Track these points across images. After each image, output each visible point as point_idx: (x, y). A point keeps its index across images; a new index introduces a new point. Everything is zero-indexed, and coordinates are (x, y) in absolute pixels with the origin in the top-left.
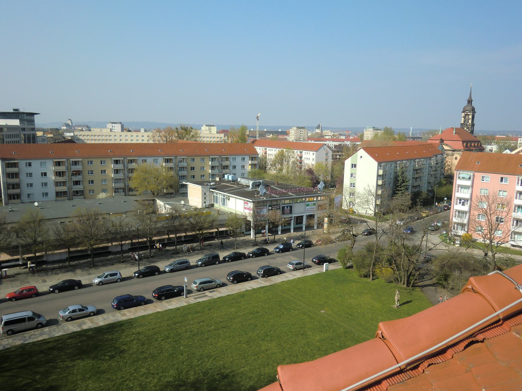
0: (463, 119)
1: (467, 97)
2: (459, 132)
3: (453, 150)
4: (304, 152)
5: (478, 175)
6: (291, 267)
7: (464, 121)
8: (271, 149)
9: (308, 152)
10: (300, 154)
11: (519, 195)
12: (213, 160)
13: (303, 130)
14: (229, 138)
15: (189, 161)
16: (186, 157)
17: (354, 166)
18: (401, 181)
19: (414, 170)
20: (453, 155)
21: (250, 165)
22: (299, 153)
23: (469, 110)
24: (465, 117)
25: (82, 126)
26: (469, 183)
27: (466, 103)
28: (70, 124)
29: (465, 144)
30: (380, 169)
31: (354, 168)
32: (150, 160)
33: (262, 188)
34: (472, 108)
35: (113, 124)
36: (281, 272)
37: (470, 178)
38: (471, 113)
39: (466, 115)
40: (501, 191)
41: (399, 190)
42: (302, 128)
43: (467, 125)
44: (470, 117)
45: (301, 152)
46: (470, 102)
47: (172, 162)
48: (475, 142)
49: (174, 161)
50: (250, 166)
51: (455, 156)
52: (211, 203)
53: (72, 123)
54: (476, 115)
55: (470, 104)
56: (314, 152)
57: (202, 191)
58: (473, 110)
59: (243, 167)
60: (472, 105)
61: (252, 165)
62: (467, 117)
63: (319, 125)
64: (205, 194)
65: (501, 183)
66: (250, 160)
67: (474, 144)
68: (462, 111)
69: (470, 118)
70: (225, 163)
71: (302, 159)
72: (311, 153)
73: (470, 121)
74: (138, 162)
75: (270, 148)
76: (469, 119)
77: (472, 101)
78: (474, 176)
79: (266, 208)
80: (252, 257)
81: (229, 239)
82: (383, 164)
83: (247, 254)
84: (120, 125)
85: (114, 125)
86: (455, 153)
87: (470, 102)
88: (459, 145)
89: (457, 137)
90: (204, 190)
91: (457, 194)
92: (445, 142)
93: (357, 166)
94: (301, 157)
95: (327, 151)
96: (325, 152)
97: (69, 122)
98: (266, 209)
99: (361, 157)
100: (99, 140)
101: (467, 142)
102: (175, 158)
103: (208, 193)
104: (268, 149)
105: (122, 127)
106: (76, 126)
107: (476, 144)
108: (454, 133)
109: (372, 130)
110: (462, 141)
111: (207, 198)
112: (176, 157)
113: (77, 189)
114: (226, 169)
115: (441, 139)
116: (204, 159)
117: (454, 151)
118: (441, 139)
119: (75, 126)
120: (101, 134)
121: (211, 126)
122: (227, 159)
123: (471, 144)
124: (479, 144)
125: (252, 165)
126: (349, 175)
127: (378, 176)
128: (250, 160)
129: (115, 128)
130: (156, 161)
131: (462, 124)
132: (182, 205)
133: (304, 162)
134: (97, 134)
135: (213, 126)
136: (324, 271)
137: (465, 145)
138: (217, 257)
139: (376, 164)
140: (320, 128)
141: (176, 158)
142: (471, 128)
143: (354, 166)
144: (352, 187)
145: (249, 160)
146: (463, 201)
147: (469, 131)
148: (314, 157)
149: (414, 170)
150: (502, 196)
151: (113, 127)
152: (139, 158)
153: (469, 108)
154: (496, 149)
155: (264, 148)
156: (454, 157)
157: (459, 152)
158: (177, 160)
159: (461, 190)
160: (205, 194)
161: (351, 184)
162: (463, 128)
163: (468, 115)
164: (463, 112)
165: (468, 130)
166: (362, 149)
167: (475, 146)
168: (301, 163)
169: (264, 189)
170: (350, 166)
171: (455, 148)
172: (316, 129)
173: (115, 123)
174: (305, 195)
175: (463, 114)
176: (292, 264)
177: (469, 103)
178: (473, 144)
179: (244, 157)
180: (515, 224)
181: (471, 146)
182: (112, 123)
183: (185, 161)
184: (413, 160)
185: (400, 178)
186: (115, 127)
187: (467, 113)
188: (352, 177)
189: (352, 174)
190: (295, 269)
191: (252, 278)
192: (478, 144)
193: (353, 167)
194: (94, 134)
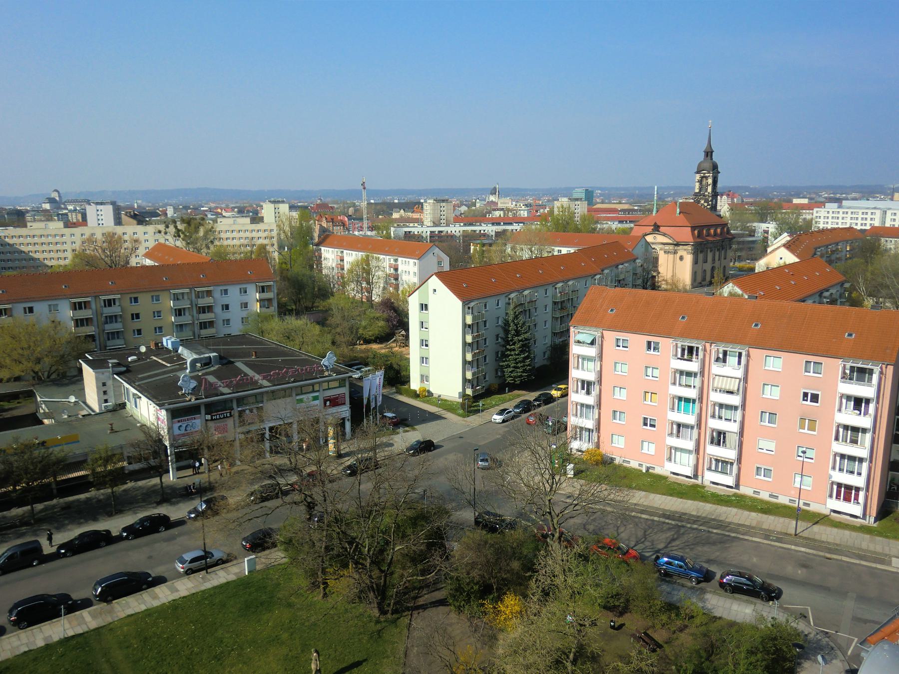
0: (697, 185)
1: (704, 146)
2: (685, 209)
3: (675, 243)
4: (400, 259)
5: (610, 336)
6: (179, 567)
7: (700, 189)
8: (350, 252)
9: (407, 260)
10: (394, 263)
11: (678, 375)
12: (176, 298)
13: (444, 204)
14: (316, 222)
15: (126, 302)
16: (118, 296)
17: (424, 307)
18: (513, 332)
19: (555, 303)
20: (675, 252)
21: (257, 301)
22: (392, 262)
23: (708, 169)
24: (700, 182)
25: (80, 202)
26: (592, 352)
27: (702, 156)
28: (57, 199)
29: (696, 232)
30: (468, 313)
31: (424, 311)
32: (41, 308)
33: (185, 379)
34: (711, 165)
35: (98, 206)
36: (160, 581)
37: (592, 343)
38: (711, 175)
39: (702, 177)
40: (650, 367)
41: (511, 350)
42: (443, 201)
43: (704, 196)
44: (710, 181)
45: (396, 260)
46: (709, 153)
47: (90, 308)
48: (716, 226)
49: (93, 306)
50: (258, 303)
51: (680, 253)
52: (119, 402)
53: (60, 196)
54: (720, 177)
55: (709, 157)
56: (416, 261)
57: (97, 379)
58: (715, 167)
59: (245, 305)
60: (712, 159)
61: (261, 300)
62: (704, 182)
63: (495, 188)
64: (104, 384)
65: (648, 352)
66: (257, 292)
67: (715, 231)
68: (696, 170)
69: (709, 183)
70: (204, 302)
71: (399, 272)
72: (411, 261)
73: (710, 189)
74: (15, 313)
75: (348, 252)
76: (708, 185)
77: (712, 152)
78: (602, 337)
79: (200, 418)
80: (127, 538)
81: (125, 487)
82: (472, 305)
83: (115, 533)
84: (110, 207)
85: (100, 207)
86: (679, 248)
87: (709, 153)
88: (686, 234)
89: (682, 219)
90: (101, 376)
91: (575, 373)
92: (662, 229)
93: (429, 307)
94: (396, 269)
95: (438, 257)
96: (435, 260)
97: (55, 195)
98: (199, 420)
99: (435, 290)
100: (42, 244)
101: (700, 228)
102: (95, 299)
103: (110, 383)
104: (345, 252)
105: (117, 210)
106: (69, 202)
107: (719, 231)
108: (678, 212)
109: (567, 200)
110: (692, 227)
111: (111, 393)
112: (96, 297)
113: (81, 316)
114: (208, 312)
115: (655, 223)
116: (158, 296)
117: (677, 245)
118: (655, 223)
119: (66, 202)
120: (45, 234)
121: (279, 202)
122: (209, 293)
123: (708, 230)
124: (725, 229)
125: (261, 300)
126: (418, 325)
127: (465, 325)
128: (257, 292)
129: (102, 213)
130: (53, 309)
131: (696, 194)
132: (72, 405)
133: (401, 278)
134: (38, 233)
135: (283, 202)
136: (247, 574)
137: (696, 234)
138: (37, 548)
139: (458, 304)
140: (497, 193)
141: (98, 299)
142: (712, 201)
143: (424, 307)
144: (424, 347)
145: (255, 291)
146: (587, 386)
147: (708, 207)
148: (416, 269)
149: (555, 303)
150: (651, 378)
151: (98, 210)
152: (15, 305)
153: (708, 165)
154: (774, 230)
155: (339, 250)
156: (678, 255)
157: (685, 247)
158: (100, 302)
159: (583, 364)
160: (104, 384)
161: (423, 340)
162: (699, 202)
163: (707, 178)
164: (698, 172)
165: (706, 204)
166: (434, 277)
167: (715, 234)
168: (396, 279)
169: (192, 381)
170: (418, 307)
171: (679, 239)
172: (491, 196)
173: (102, 204)
174: (294, 382)
175: (698, 177)
176: (183, 562)
177: (707, 156)
178: (712, 231)
179: (244, 286)
180: (675, 431)
181: (709, 235)
182: (97, 204)
183: (117, 304)
184: (551, 286)
185: (512, 327)
186: (101, 210)
187: (705, 173)
188: (422, 328)
189: (422, 322)
190: (189, 572)
191: (74, 607)
192: (722, 229)
193: (422, 310)
194: (31, 234)
